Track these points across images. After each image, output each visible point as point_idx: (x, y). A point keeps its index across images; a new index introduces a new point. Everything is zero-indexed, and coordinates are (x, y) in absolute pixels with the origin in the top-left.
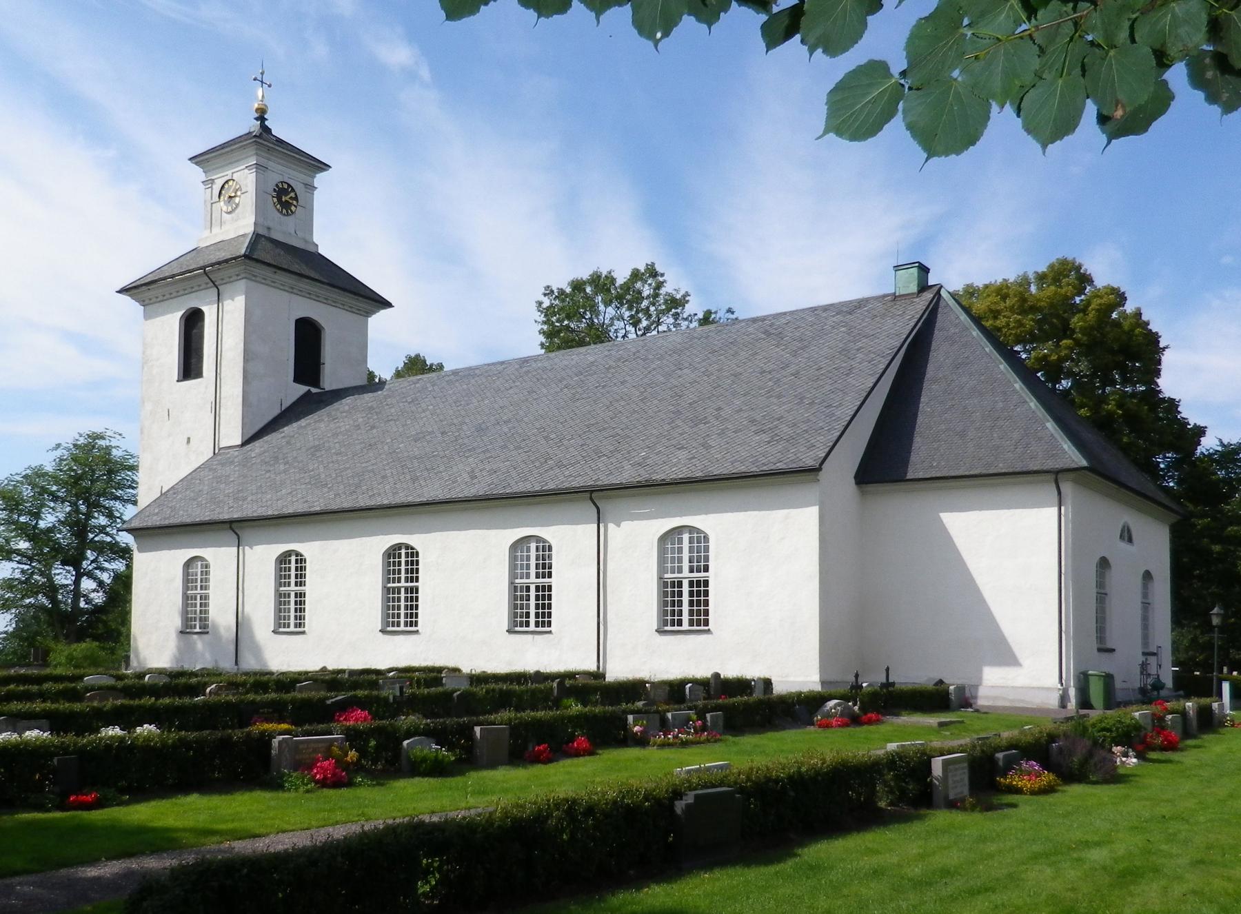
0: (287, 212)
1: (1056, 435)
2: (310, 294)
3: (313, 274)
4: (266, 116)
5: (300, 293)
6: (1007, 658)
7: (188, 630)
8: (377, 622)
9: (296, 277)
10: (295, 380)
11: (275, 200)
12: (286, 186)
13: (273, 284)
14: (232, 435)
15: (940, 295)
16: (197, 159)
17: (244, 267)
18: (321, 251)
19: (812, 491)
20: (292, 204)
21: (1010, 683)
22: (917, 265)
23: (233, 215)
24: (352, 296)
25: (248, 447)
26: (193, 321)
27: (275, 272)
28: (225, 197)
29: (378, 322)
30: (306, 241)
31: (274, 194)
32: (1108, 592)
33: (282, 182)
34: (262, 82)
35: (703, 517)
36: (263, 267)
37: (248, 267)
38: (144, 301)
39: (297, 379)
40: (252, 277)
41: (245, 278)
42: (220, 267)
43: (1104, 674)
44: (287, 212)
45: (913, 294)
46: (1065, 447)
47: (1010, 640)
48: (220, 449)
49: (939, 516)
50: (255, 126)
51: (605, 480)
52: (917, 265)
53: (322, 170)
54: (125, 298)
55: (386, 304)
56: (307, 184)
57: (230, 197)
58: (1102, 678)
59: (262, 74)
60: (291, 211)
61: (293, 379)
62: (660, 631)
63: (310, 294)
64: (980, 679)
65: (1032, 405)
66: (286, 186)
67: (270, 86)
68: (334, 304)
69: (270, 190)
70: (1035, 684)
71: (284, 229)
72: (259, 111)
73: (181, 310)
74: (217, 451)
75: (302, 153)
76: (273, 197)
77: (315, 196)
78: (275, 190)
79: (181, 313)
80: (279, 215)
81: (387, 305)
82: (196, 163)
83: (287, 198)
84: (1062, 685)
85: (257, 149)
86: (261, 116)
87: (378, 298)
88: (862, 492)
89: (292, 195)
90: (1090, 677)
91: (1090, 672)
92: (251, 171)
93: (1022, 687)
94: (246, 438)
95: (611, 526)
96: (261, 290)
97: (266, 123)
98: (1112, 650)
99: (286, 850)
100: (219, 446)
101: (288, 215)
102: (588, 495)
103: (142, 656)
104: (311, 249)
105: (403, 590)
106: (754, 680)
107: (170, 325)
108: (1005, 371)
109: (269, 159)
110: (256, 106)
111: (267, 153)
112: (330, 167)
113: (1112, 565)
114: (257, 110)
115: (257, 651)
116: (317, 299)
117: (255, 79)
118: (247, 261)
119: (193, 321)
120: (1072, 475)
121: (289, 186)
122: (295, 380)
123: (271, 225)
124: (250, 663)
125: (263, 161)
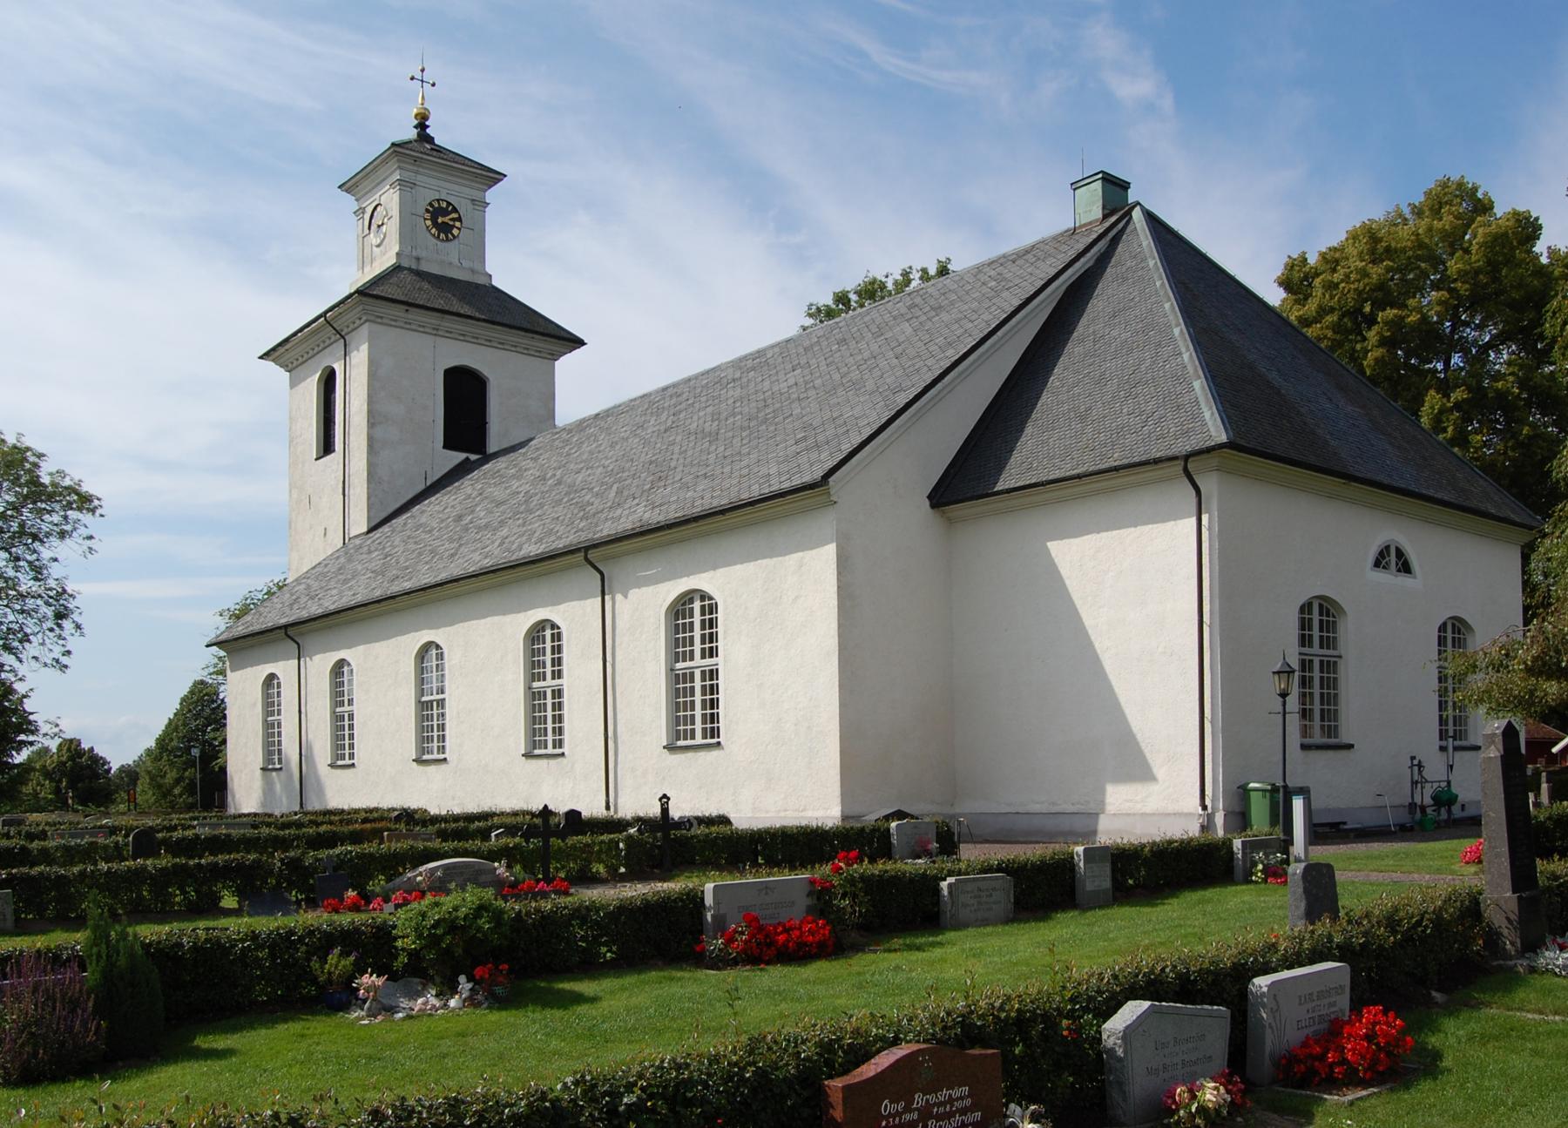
0: (447, 237)
1: (1202, 400)
3: (466, 310)
4: (427, 123)
5: (449, 335)
6: (1137, 769)
7: (270, 767)
8: (519, 743)
9: (439, 315)
10: (446, 446)
11: (429, 223)
13: (408, 326)
14: (359, 524)
15: (1131, 216)
16: (349, 187)
17: (361, 307)
18: (497, 282)
19: (827, 521)
20: (454, 226)
21: (1139, 808)
22: (1100, 176)
23: (381, 248)
24: (523, 333)
25: (377, 534)
26: (328, 382)
28: (374, 227)
29: (567, 366)
30: (473, 271)
31: (428, 216)
32: (1343, 653)
33: (438, 200)
34: (422, 81)
35: (710, 574)
36: (384, 303)
37: (367, 307)
38: (287, 366)
39: (449, 444)
40: (377, 320)
41: (366, 321)
42: (341, 311)
43: (1269, 787)
44: (447, 237)
45: (1097, 220)
46: (1207, 415)
47: (1139, 737)
48: (350, 539)
49: (1047, 547)
50: (412, 134)
51: (607, 530)
52: (1100, 176)
54: (269, 365)
55: (577, 343)
56: (473, 200)
57: (379, 226)
58: (1268, 794)
59: (423, 70)
62: (671, 748)
63: (463, 335)
64: (1102, 803)
65: (1186, 356)
66: (444, 205)
67: (433, 85)
68: (502, 345)
69: (421, 211)
70: (1171, 808)
71: (444, 259)
73: (316, 372)
74: (347, 541)
75: (470, 163)
78: (427, 211)
79: (318, 375)
80: (435, 241)
81: (577, 343)
82: (347, 191)
83: (446, 219)
84: (1204, 808)
85: (399, 161)
86: (422, 126)
87: (563, 334)
88: (949, 519)
89: (454, 215)
90: (1251, 793)
91: (1252, 785)
93: (1154, 814)
94: (373, 524)
95: (619, 597)
96: (392, 336)
97: (428, 131)
98: (1351, 746)
99: (206, 1061)
101: (448, 240)
102: (580, 556)
104: (481, 280)
105: (435, 703)
107: (311, 387)
108: (1169, 312)
109: (417, 172)
110: (415, 111)
111: (414, 165)
112: (505, 176)
113: (1346, 609)
114: (416, 116)
115: (320, 791)
116: (475, 340)
117: (412, 78)
118: (364, 299)
119: (328, 382)
120: (1213, 460)
121: (449, 204)
122: (446, 446)
123: (423, 254)
124: (314, 805)
125: (408, 176)
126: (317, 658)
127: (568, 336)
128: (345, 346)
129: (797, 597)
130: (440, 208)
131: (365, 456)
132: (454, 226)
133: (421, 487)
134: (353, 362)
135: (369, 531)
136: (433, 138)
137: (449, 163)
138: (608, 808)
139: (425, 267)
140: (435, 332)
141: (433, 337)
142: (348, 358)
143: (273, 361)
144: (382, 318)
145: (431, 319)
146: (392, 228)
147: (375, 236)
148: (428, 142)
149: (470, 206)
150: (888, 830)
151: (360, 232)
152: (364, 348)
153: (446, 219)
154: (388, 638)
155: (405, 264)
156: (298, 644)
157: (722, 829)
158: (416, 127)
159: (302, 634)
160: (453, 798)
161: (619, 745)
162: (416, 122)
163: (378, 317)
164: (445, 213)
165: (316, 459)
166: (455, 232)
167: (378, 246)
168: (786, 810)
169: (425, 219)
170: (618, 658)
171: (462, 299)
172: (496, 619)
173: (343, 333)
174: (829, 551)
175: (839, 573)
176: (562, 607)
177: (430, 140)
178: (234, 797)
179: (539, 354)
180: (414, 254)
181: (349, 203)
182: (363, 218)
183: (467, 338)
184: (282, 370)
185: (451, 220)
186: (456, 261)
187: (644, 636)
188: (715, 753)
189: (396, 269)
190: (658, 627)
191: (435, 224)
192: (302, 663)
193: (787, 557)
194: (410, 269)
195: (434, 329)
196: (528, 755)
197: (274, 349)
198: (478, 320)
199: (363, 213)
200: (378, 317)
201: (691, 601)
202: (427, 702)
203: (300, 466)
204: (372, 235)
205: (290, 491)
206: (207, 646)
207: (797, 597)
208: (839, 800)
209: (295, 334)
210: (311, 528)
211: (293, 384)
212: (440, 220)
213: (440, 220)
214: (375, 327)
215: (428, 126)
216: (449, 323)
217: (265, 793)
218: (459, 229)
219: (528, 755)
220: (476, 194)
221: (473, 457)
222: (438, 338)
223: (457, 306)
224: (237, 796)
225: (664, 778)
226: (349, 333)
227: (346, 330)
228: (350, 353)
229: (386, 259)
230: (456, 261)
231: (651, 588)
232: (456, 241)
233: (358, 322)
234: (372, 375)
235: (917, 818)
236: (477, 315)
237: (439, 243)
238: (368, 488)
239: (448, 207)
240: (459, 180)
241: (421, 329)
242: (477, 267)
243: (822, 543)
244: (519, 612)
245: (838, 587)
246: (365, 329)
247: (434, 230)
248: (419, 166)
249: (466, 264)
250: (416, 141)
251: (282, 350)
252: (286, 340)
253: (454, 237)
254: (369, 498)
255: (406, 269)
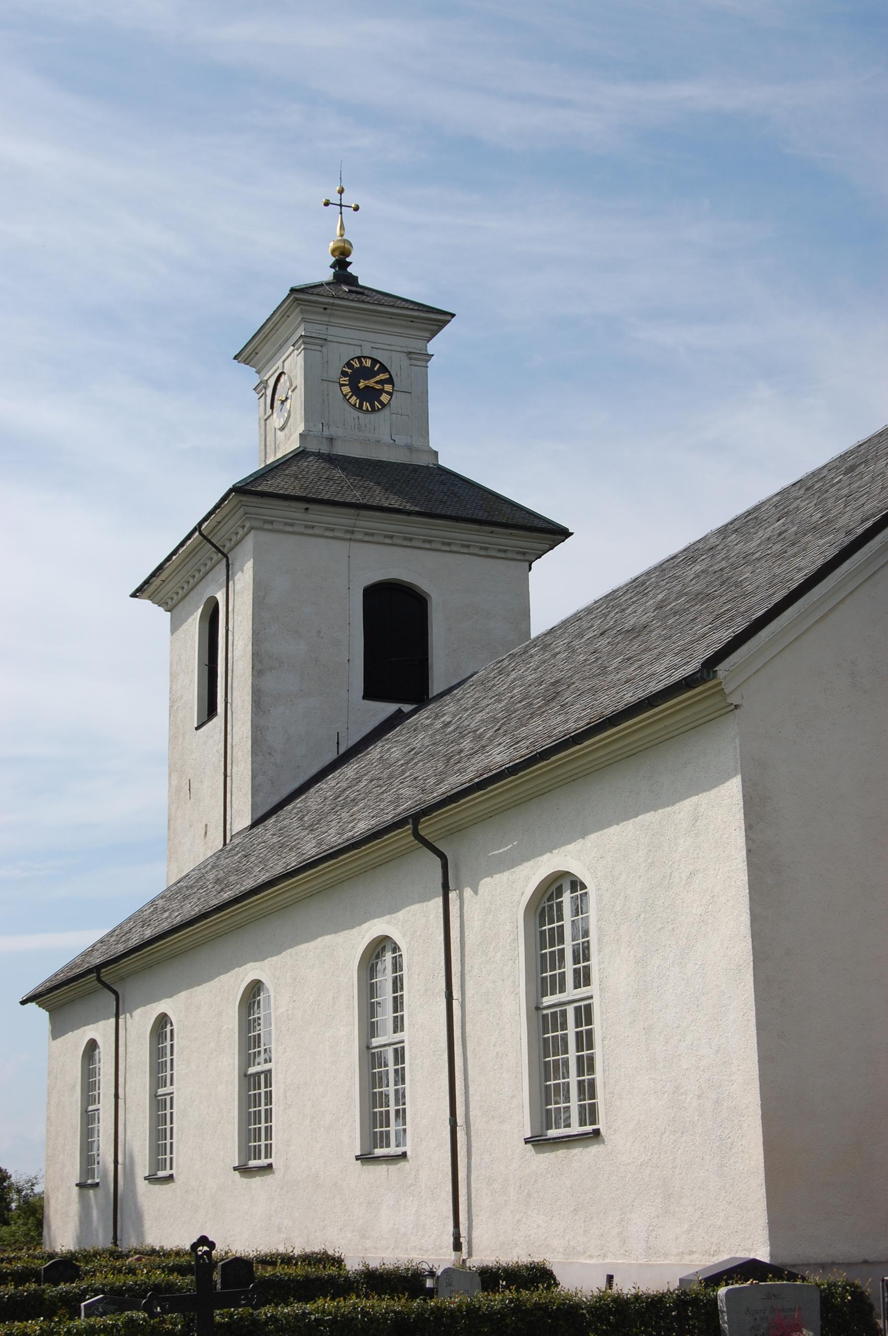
0: (373, 406)
2: (391, 537)
3: (394, 502)
4: (348, 260)
5: (369, 538)
7: (89, 1182)
9: (352, 511)
10: (368, 695)
11: (346, 390)
12: (368, 363)
13: (311, 531)
14: (242, 819)
17: (241, 511)
18: (443, 462)
23: (286, 429)
24: (477, 527)
25: (260, 829)
27: (307, 509)
28: (277, 403)
30: (410, 448)
31: (345, 380)
33: (359, 358)
34: (341, 205)
39: (372, 692)
40: (267, 525)
41: (252, 528)
42: (219, 518)
50: (327, 275)
53: (442, 324)
54: (145, 605)
55: (560, 534)
56: (410, 353)
59: (341, 192)
60: (381, 403)
61: (362, 694)
63: (391, 537)
66: (368, 363)
67: (356, 209)
68: (447, 546)
69: (335, 374)
72: (337, 253)
73: (199, 608)
74: (228, 842)
76: (342, 385)
77: (430, 371)
78: (344, 374)
79: (200, 610)
80: (356, 413)
81: (560, 534)
82: (246, 362)
83: (371, 383)
85: (302, 311)
89: (382, 376)
92: (300, 350)
94: (260, 813)
95: (468, 892)
97: (350, 269)
100: (231, 833)
101: (374, 410)
102: (405, 833)
103: (52, 1233)
104: (423, 460)
106: (432, 1274)
107: (193, 625)
110: (331, 245)
112: (453, 315)
114: (333, 251)
116: (408, 542)
117: (327, 204)
118: (244, 499)
121: (375, 361)
122: (368, 695)
123: (333, 431)
125: (317, 330)
126: (138, 1013)
127: (545, 525)
128: (228, 565)
129: (692, 874)
130: (363, 368)
131: (249, 717)
132: (382, 391)
133: (331, 756)
134: (238, 587)
135: (255, 824)
136: (356, 278)
137: (371, 307)
138: (457, 1246)
139: (341, 450)
140: (348, 536)
141: (347, 544)
142: (231, 583)
143: (149, 598)
144: (272, 522)
145: (342, 519)
146: (297, 403)
147: (278, 417)
148: (347, 283)
149: (405, 362)
150: (714, 1301)
151: (262, 412)
152: (249, 566)
153: (371, 383)
154: (210, 978)
155: (313, 447)
156: (116, 993)
157: (532, 1297)
158: (333, 267)
159: (122, 979)
160: (280, 1230)
161: (473, 1138)
162: (333, 259)
163: (265, 522)
164: (368, 373)
165: (197, 729)
166: (384, 398)
167: (282, 429)
168: (691, 1253)
169: (342, 385)
170: (469, 993)
171: (389, 488)
172: (327, 939)
173: (225, 551)
174: (734, 787)
175: (749, 828)
176: (401, 914)
177: (352, 280)
178: (49, 1227)
179: (503, 554)
180: (326, 433)
181: (248, 376)
182: (265, 394)
183: (395, 541)
184: (161, 609)
185: (377, 382)
186: (386, 438)
187: (499, 955)
188: (594, 1150)
189: (299, 455)
190: (516, 940)
191: (356, 390)
192: (121, 1021)
193: (677, 807)
194: (319, 455)
195: (347, 531)
196: (365, 1158)
197: (147, 582)
198: (409, 513)
199: (265, 388)
200: (265, 522)
201: (559, 892)
202: (258, 1074)
203: (180, 740)
204: (275, 415)
205: (170, 775)
206: (23, 1003)
207: (692, 874)
208: (766, 1233)
209: (169, 559)
210: (191, 826)
211: (174, 627)
212: (362, 385)
213: (362, 385)
214: (264, 536)
215: (350, 263)
216: (368, 522)
217: (81, 1223)
218: (390, 394)
219: (365, 1158)
220: (414, 345)
221: (407, 708)
222: (353, 544)
223: (379, 497)
224: (53, 1227)
225: (529, 1195)
226: (232, 549)
227: (228, 545)
228: (234, 575)
229: (289, 444)
230: (386, 438)
231: (506, 874)
232: (386, 411)
233: (241, 532)
234: (259, 604)
235: (792, 1277)
236: (409, 507)
237: (361, 415)
238: (253, 762)
239: (373, 365)
240: (378, 327)
241: (329, 533)
242: (417, 442)
243: (722, 778)
244: (353, 927)
245: (749, 851)
246: (249, 543)
247: (353, 399)
248: (330, 315)
249: (401, 440)
250: (328, 284)
251: (157, 582)
252: (160, 568)
253: (384, 405)
254: (254, 777)
255: (313, 454)
